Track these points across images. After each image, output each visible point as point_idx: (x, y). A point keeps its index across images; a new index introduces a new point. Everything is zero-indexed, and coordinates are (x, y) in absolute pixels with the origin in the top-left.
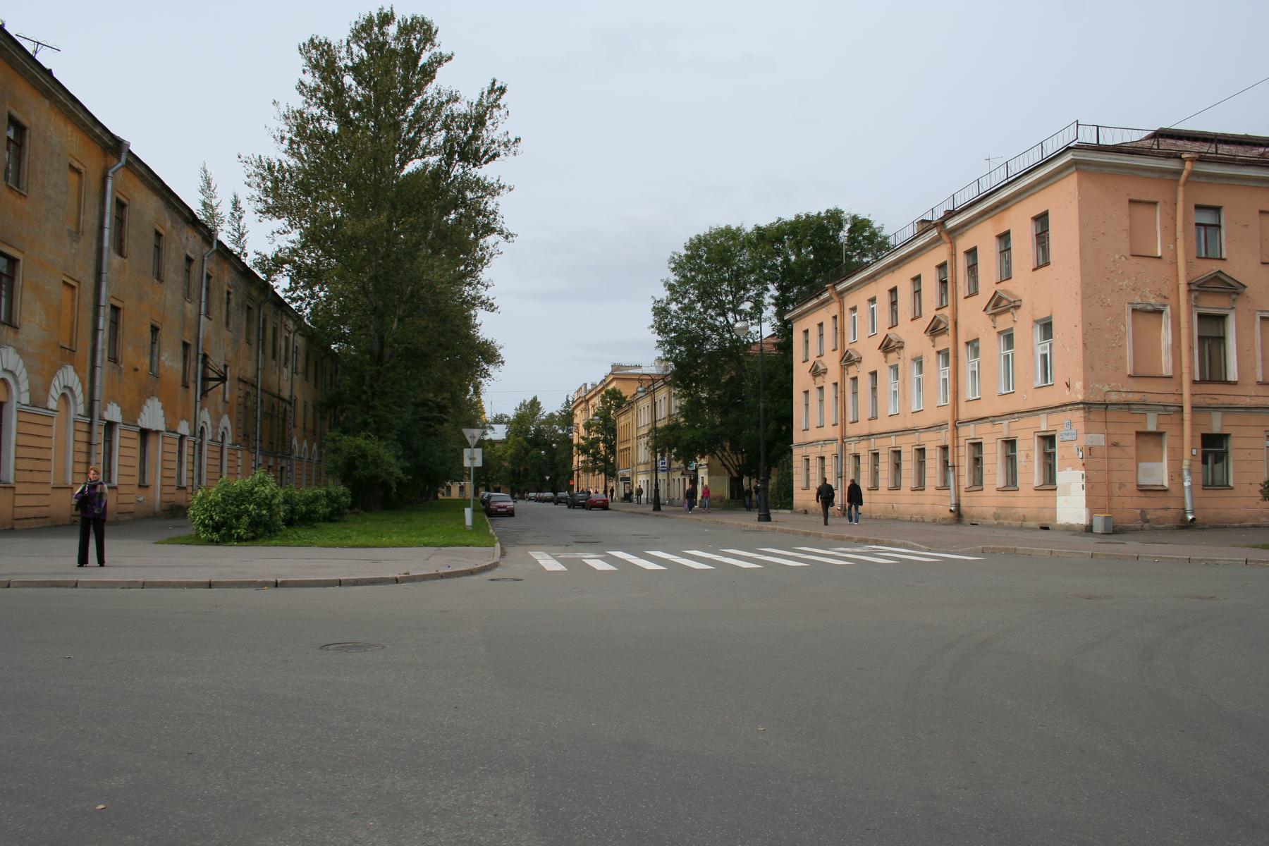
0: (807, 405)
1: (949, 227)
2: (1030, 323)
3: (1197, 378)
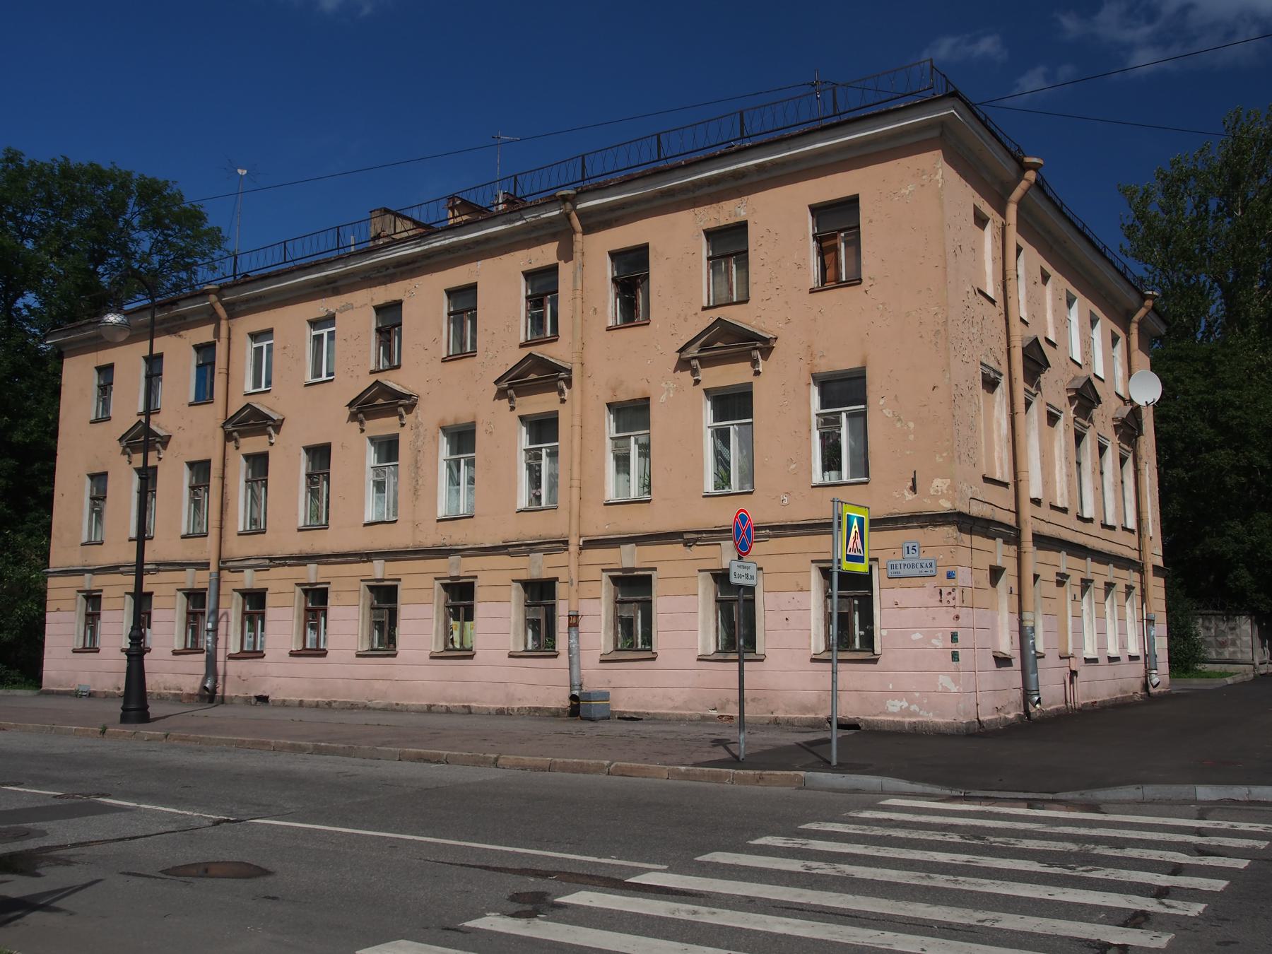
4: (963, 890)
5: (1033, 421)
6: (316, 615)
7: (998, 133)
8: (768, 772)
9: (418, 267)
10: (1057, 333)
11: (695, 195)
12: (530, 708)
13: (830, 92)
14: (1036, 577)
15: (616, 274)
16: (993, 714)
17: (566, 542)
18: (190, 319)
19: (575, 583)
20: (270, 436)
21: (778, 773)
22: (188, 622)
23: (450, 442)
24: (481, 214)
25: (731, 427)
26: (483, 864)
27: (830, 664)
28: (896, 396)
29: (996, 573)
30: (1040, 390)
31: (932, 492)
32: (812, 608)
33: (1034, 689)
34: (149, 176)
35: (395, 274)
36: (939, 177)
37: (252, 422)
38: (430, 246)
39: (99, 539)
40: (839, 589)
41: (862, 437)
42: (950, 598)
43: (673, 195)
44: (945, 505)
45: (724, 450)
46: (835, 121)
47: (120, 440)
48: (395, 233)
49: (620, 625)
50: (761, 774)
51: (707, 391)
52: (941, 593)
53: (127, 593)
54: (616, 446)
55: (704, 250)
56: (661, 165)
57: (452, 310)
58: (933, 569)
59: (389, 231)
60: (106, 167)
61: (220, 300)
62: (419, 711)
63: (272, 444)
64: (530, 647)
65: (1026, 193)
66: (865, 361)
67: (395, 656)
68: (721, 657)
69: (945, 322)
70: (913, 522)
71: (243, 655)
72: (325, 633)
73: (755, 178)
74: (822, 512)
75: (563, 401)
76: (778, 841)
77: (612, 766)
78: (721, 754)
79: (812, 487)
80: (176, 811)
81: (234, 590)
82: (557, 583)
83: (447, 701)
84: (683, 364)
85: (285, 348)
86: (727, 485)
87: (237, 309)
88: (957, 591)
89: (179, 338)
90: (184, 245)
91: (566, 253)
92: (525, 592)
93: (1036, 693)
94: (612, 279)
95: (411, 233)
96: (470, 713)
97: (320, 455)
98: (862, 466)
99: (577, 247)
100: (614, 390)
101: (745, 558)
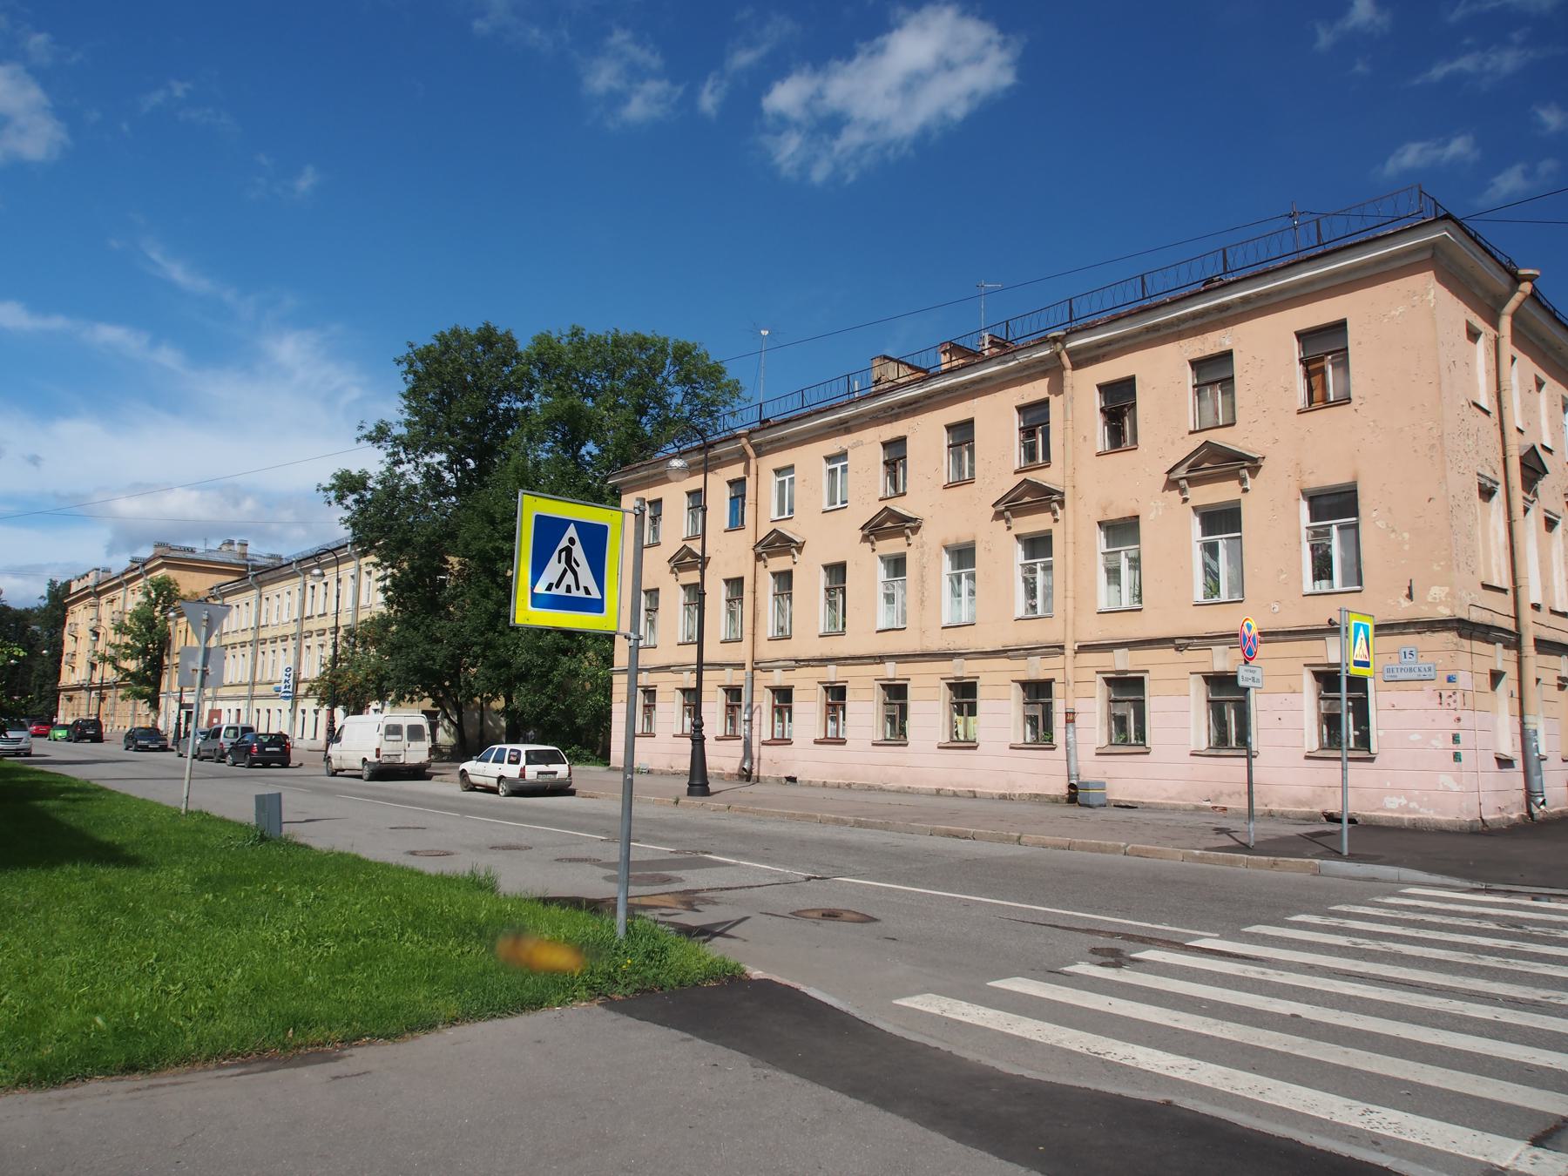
4: (1516, 971)
5: (1530, 527)
6: (835, 709)
7: (1494, 252)
8: (1281, 859)
9: (920, 407)
10: (1553, 439)
11: (1180, 328)
12: (1030, 794)
13: (1313, 226)
14: (1538, 680)
15: (1103, 405)
16: (1495, 814)
17: (1062, 647)
18: (723, 459)
19: (1071, 683)
20: (794, 556)
21: (1292, 860)
22: (727, 713)
23: (952, 559)
24: (973, 357)
25: (1220, 541)
26: (1053, 924)
27: (1340, 762)
28: (1389, 508)
29: (1496, 677)
30: (1537, 497)
31: (1430, 599)
32: (1305, 708)
33: (1538, 790)
34: (682, 340)
35: (899, 413)
36: (1431, 297)
37: (778, 544)
38: (932, 387)
39: (652, 644)
40: (1348, 691)
41: (1354, 548)
42: (1451, 701)
43: (1159, 330)
44: (1444, 612)
45: (1208, 559)
46: (1320, 251)
47: (669, 561)
48: (898, 378)
49: (1113, 722)
50: (1275, 861)
51: (1195, 509)
52: (1440, 696)
53: (677, 689)
54: (1107, 560)
55: (1189, 378)
56: (1146, 303)
57: (951, 442)
58: (1432, 673)
59: (893, 376)
60: (648, 335)
61: (749, 442)
62: (929, 794)
63: (795, 563)
64: (1028, 740)
65: (1521, 304)
66: (1356, 475)
67: (906, 745)
68: (1214, 752)
69: (1441, 436)
70: (1409, 628)
71: (774, 742)
72: (844, 725)
73: (1240, 310)
74: (1317, 615)
75: (1056, 521)
76: (1315, 920)
77: (1129, 847)
78: (1226, 841)
79: (1304, 596)
80: (769, 867)
81: (766, 687)
82: (1053, 683)
83: (953, 786)
84: (1172, 484)
85: (804, 481)
86: (1216, 594)
87: (763, 449)
88: (1458, 694)
89: (715, 476)
90: (709, 396)
91: (1057, 388)
92: (1024, 691)
93: (1540, 794)
95: (912, 378)
96: (975, 797)
97: (837, 572)
98: (1356, 575)
99: (1067, 382)
100: (1104, 510)
101: (1251, 663)
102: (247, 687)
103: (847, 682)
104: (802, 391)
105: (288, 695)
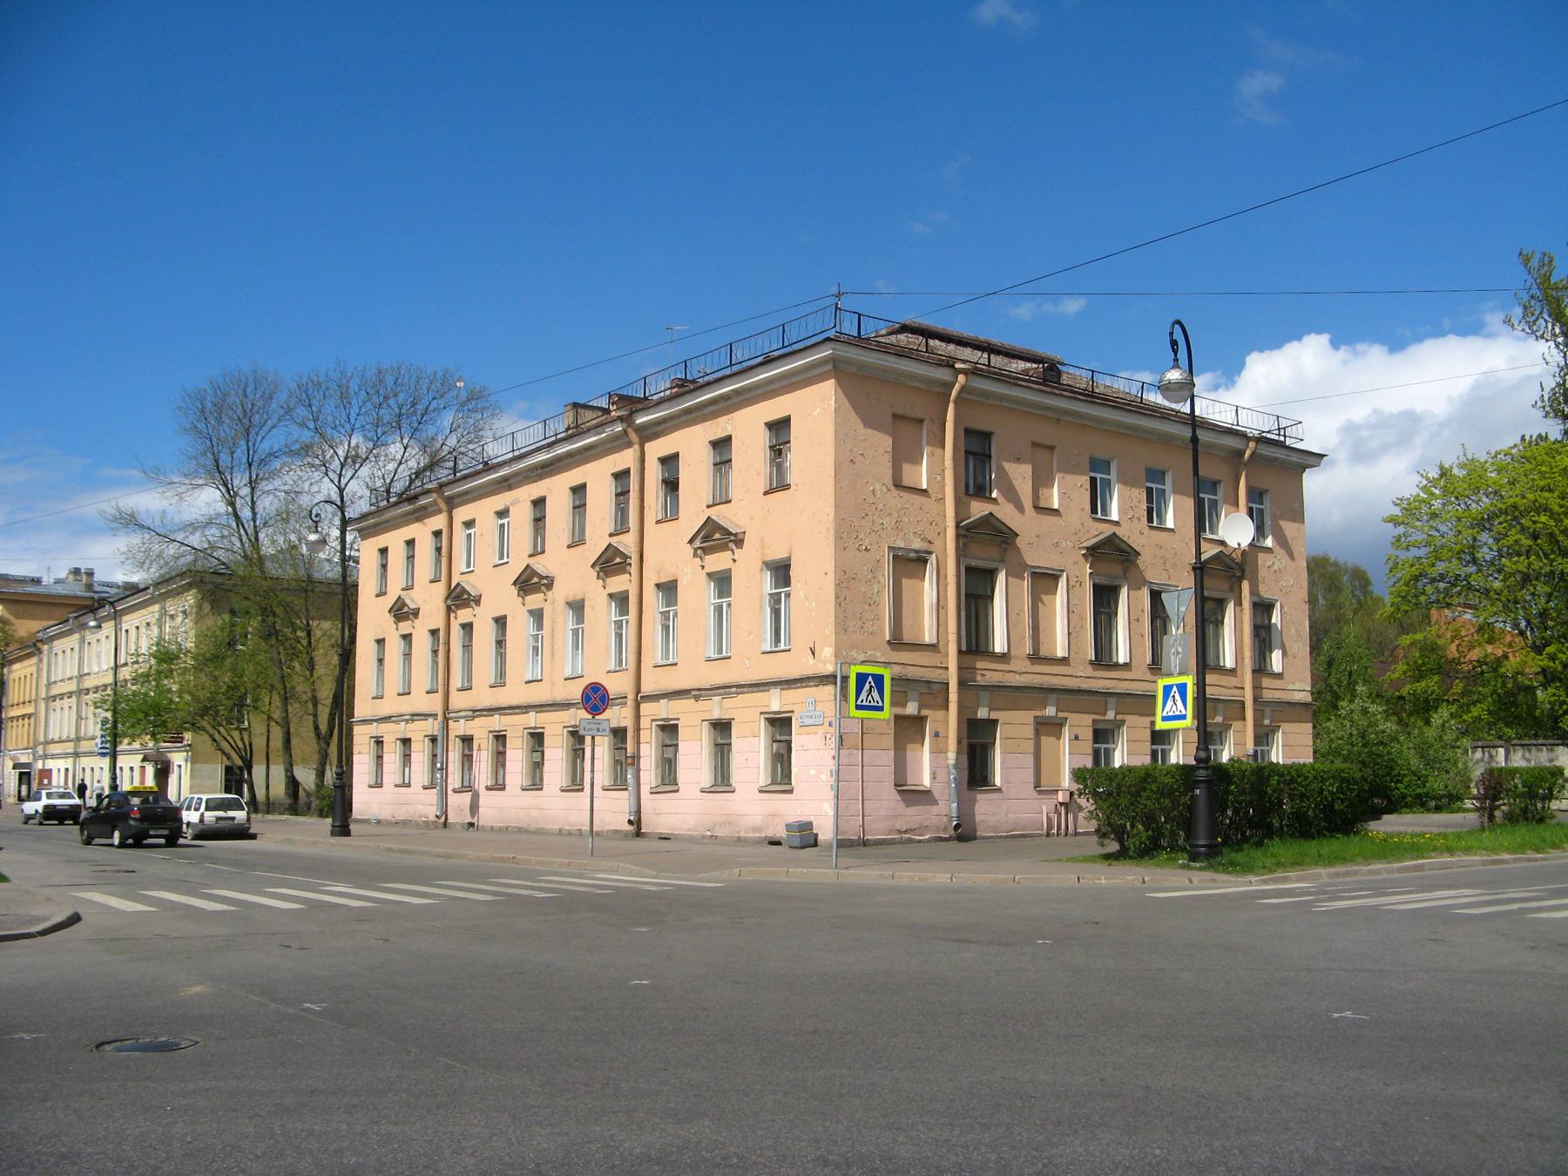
0: (381, 661)
1: (637, 422)
2: (759, 564)
3: (964, 648)
20: (732, 551)
53: (398, 739)
67: (541, 789)
94: (663, 480)
96: (581, 835)
100: (659, 573)
102: (72, 743)
103: (544, 728)
104: (645, 378)
105: (104, 751)
